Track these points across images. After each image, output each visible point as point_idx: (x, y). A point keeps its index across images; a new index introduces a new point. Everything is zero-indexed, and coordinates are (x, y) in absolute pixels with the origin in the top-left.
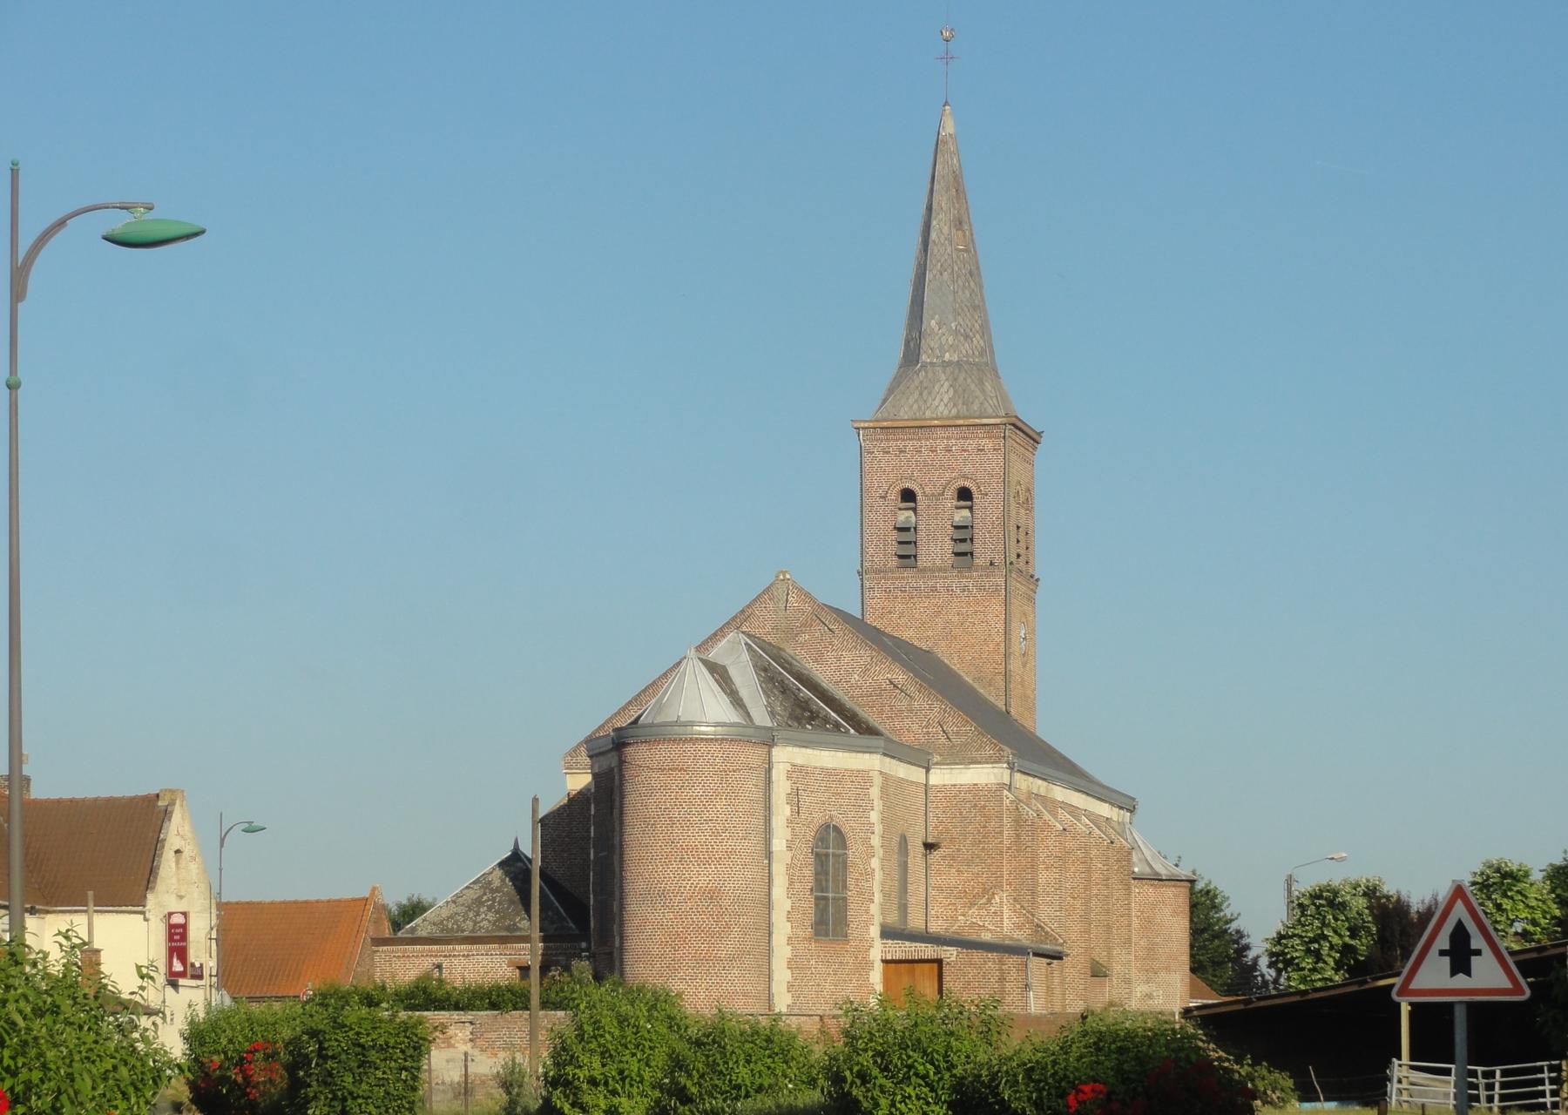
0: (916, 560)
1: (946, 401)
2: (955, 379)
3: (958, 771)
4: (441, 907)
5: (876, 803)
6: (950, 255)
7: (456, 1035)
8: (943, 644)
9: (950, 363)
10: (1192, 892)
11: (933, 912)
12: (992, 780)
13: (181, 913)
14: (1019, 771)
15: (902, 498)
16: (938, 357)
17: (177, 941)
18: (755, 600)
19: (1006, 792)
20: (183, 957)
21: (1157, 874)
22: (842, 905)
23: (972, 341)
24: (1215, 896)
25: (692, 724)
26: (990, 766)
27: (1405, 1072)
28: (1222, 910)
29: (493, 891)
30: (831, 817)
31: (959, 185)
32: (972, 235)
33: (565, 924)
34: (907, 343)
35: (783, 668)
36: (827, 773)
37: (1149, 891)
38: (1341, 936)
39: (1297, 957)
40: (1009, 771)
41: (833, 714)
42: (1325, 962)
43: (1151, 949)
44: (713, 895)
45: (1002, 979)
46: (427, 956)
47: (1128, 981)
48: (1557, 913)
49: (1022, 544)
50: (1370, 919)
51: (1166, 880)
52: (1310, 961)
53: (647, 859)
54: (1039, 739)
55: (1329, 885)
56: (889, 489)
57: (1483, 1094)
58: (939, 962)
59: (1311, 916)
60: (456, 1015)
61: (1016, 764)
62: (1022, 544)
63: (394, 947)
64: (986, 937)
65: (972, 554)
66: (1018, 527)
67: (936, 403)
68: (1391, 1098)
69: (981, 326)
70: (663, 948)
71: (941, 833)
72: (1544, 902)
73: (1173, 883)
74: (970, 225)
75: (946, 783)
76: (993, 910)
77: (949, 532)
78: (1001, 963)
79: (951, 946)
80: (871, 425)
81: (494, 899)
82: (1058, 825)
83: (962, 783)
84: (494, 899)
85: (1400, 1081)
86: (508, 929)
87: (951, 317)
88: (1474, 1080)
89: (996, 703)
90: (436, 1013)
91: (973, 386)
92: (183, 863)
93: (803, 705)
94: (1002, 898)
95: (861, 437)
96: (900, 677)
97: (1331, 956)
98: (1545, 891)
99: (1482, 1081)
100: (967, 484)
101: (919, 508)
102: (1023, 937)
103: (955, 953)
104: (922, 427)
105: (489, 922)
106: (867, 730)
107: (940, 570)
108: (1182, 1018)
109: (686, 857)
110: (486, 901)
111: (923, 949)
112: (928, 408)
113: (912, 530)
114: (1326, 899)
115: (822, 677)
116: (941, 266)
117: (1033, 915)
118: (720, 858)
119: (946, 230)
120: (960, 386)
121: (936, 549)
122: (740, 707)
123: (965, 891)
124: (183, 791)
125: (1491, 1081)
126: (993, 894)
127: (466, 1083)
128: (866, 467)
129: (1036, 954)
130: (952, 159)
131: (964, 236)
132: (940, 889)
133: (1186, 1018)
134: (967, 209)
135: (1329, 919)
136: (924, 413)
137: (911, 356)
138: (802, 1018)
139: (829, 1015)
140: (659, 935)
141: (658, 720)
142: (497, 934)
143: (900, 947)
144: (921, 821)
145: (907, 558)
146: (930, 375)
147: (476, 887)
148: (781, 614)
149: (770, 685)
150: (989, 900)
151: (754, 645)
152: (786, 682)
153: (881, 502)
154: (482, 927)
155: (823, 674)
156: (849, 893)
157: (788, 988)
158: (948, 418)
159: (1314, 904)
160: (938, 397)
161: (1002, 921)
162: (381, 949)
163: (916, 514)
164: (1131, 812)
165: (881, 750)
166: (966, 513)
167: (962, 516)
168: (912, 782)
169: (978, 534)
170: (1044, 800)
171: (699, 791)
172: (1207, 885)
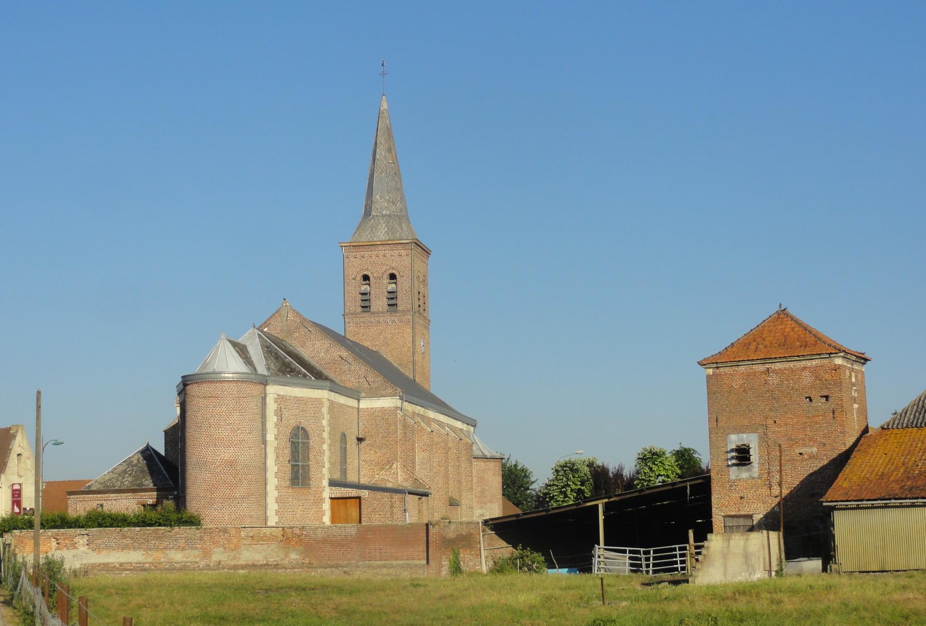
1: (383, 233)
3: (375, 401)
4: (105, 475)
5: (325, 415)
6: (386, 165)
7: (79, 542)
8: (383, 348)
9: (386, 215)
10: (504, 466)
11: (362, 473)
12: (392, 405)
13: (19, 484)
14: (406, 401)
17: (16, 497)
19: (399, 411)
20: (19, 505)
21: (485, 455)
22: (306, 468)
25: (220, 373)
27: (602, 552)
28: (529, 478)
29: (133, 466)
30: (300, 422)
32: (396, 155)
33: (168, 482)
35: (279, 347)
36: (298, 400)
37: (481, 464)
38: (576, 485)
39: (556, 495)
40: (401, 401)
41: (303, 370)
42: (569, 498)
43: (483, 492)
44: (232, 464)
45: (392, 507)
46: (95, 500)
47: (471, 508)
48: (679, 471)
49: (422, 301)
50: (590, 477)
51: (490, 458)
52: (562, 497)
54: (431, 394)
57: (644, 563)
58: (359, 498)
60: (78, 531)
62: (422, 301)
63: (78, 496)
64: (389, 485)
65: (396, 305)
66: (419, 293)
67: (379, 233)
68: (594, 566)
69: (401, 198)
72: (672, 467)
73: (493, 460)
77: (386, 295)
78: (391, 498)
79: (366, 490)
80: (348, 244)
81: (133, 470)
82: (429, 429)
84: (133, 470)
85: (599, 557)
86: (138, 485)
87: (386, 194)
88: (639, 556)
90: (67, 530)
91: (396, 226)
92: (22, 460)
94: (397, 465)
96: (344, 353)
98: (672, 461)
99: (643, 556)
100: (394, 272)
102: (408, 485)
103: (367, 493)
104: (372, 245)
106: (319, 376)
108: (483, 525)
110: (129, 471)
116: (381, 170)
117: (413, 474)
118: (236, 444)
119: (383, 153)
121: (379, 303)
122: (249, 364)
124: (23, 426)
125: (648, 556)
126: (393, 463)
128: (346, 265)
129: (410, 493)
130: (386, 121)
131: (392, 156)
132: (366, 461)
133: (486, 525)
137: (368, 213)
139: (287, 527)
141: (204, 371)
142: (132, 488)
144: (355, 426)
146: (376, 221)
147: (124, 464)
149: (270, 355)
150: (391, 467)
151: (262, 335)
152: (279, 353)
153: (353, 281)
155: (306, 353)
156: (311, 463)
157: (276, 513)
158: (385, 241)
159: (563, 470)
161: (397, 477)
162: (71, 497)
164: (474, 427)
166: (394, 285)
167: (392, 287)
168: (349, 406)
169: (399, 295)
170: (423, 417)
171: (224, 408)
172: (522, 467)
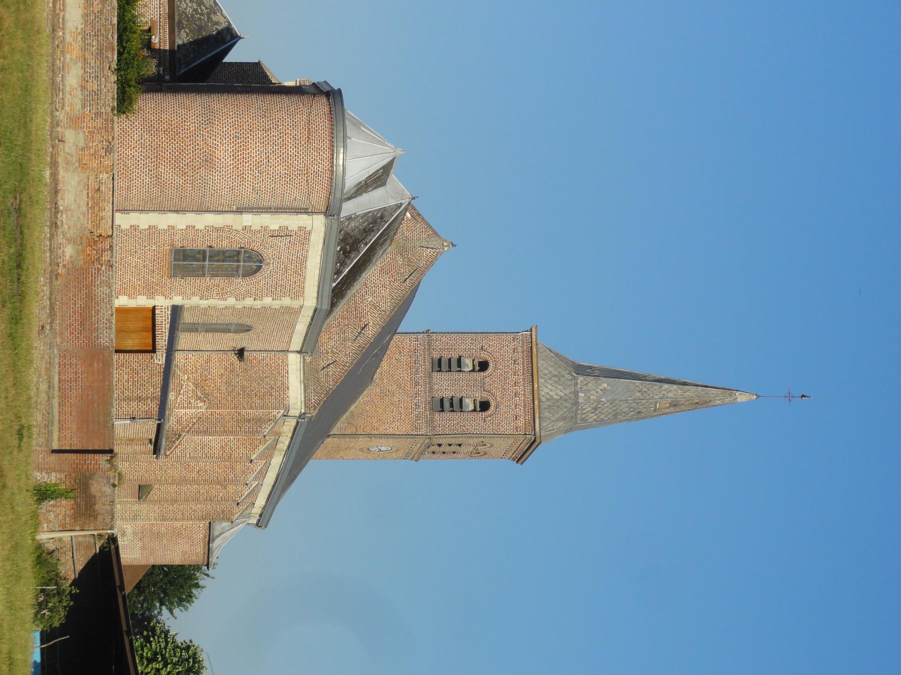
0: (437, 371)
1: (551, 393)
2: (566, 401)
3: (299, 375)
5: (278, 302)
9: (577, 396)
11: (190, 356)
12: (292, 401)
14: (298, 422)
15: (481, 362)
16: (581, 388)
18: (428, 224)
19: (282, 411)
21: (213, 541)
22: (200, 273)
23: (592, 413)
24: (188, 601)
25: (345, 147)
26: (303, 399)
30: (268, 264)
31: (702, 404)
32: (666, 414)
34: (590, 367)
36: (302, 262)
37: (200, 534)
39: (151, 646)
41: (347, 270)
42: (147, 666)
43: (158, 536)
44: (209, 162)
45: (139, 399)
47: (135, 518)
49: (448, 449)
53: (237, 111)
55: (202, 668)
56: (488, 352)
58: (154, 350)
59: (181, 655)
61: (303, 420)
62: (448, 449)
64: (171, 396)
65: (443, 411)
66: (460, 445)
67: (549, 387)
70: (166, 122)
71: (251, 362)
73: (206, 552)
74: (672, 413)
75: (289, 366)
76: (192, 401)
77: (458, 395)
80: (534, 340)
81: (202, 14)
83: (290, 378)
86: (180, 22)
87: (609, 398)
89: (336, 428)
91: (561, 413)
93: (355, 247)
94: (201, 408)
95: (525, 333)
96: (371, 332)
97: (151, 670)
100: (492, 408)
101: (475, 374)
102: (171, 424)
103: (160, 363)
105: (185, 9)
106: (338, 293)
107: (431, 388)
109: (239, 141)
110: (201, 9)
111: (164, 338)
112: (546, 380)
113: (459, 369)
114: (193, 666)
115: (369, 274)
116: (645, 392)
118: (238, 168)
120: (562, 403)
122: (357, 191)
123: (207, 380)
126: (204, 401)
128: (504, 336)
129: (159, 426)
130: (719, 400)
131: (666, 408)
132: (208, 361)
134: (685, 410)
135: (179, 668)
136: (542, 378)
137: (581, 370)
138: (111, 221)
140: (177, 119)
141: (347, 123)
143: (165, 320)
145: (438, 365)
146: (569, 383)
148: (418, 244)
150: (199, 398)
152: (372, 234)
154: (181, 3)
155: (371, 274)
156: (208, 279)
158: (539, 394)
159: (189, 658)
160: (553, 388)
161: (184, 408)
163: (470, 371)
164: (257, 524)
165: (319, 307)
166: (471, 407)
167: (469, 404)
169: (457, 416)
170: (273, 447)
171: (292, 151)
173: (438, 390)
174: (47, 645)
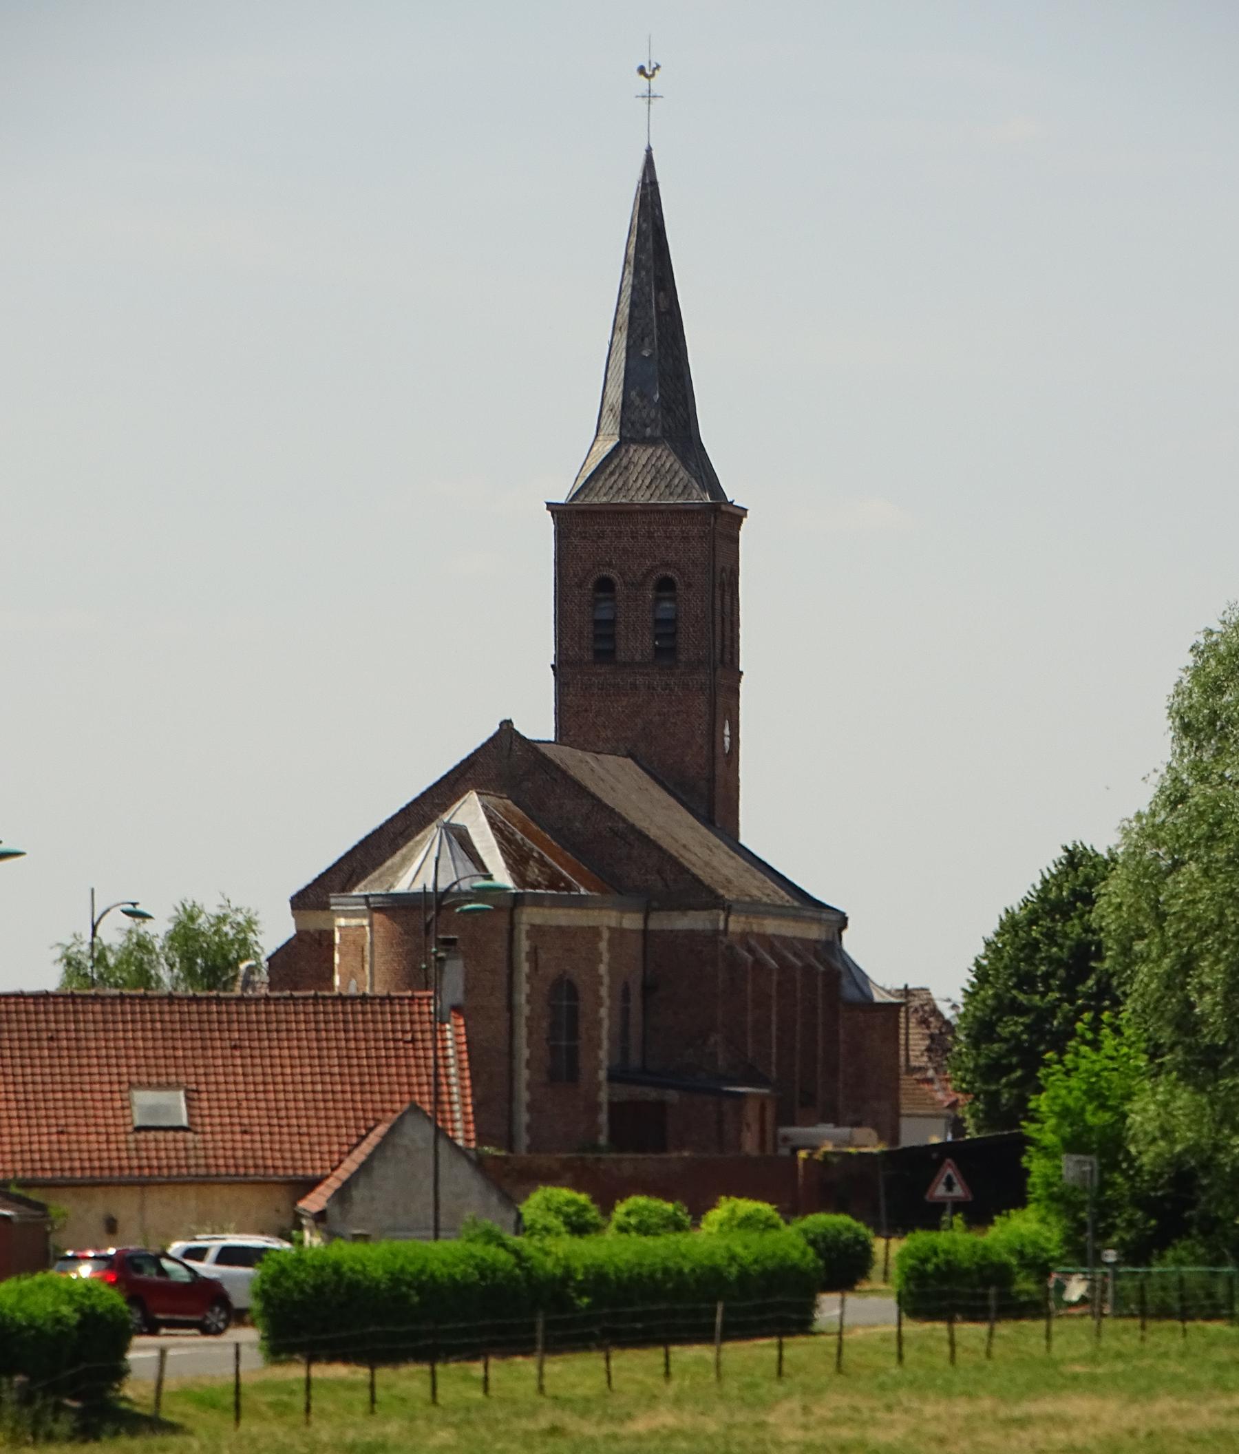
30: (565, 972)
127: (238, 1385)
173: (642, 655)
174: (567, 875)
